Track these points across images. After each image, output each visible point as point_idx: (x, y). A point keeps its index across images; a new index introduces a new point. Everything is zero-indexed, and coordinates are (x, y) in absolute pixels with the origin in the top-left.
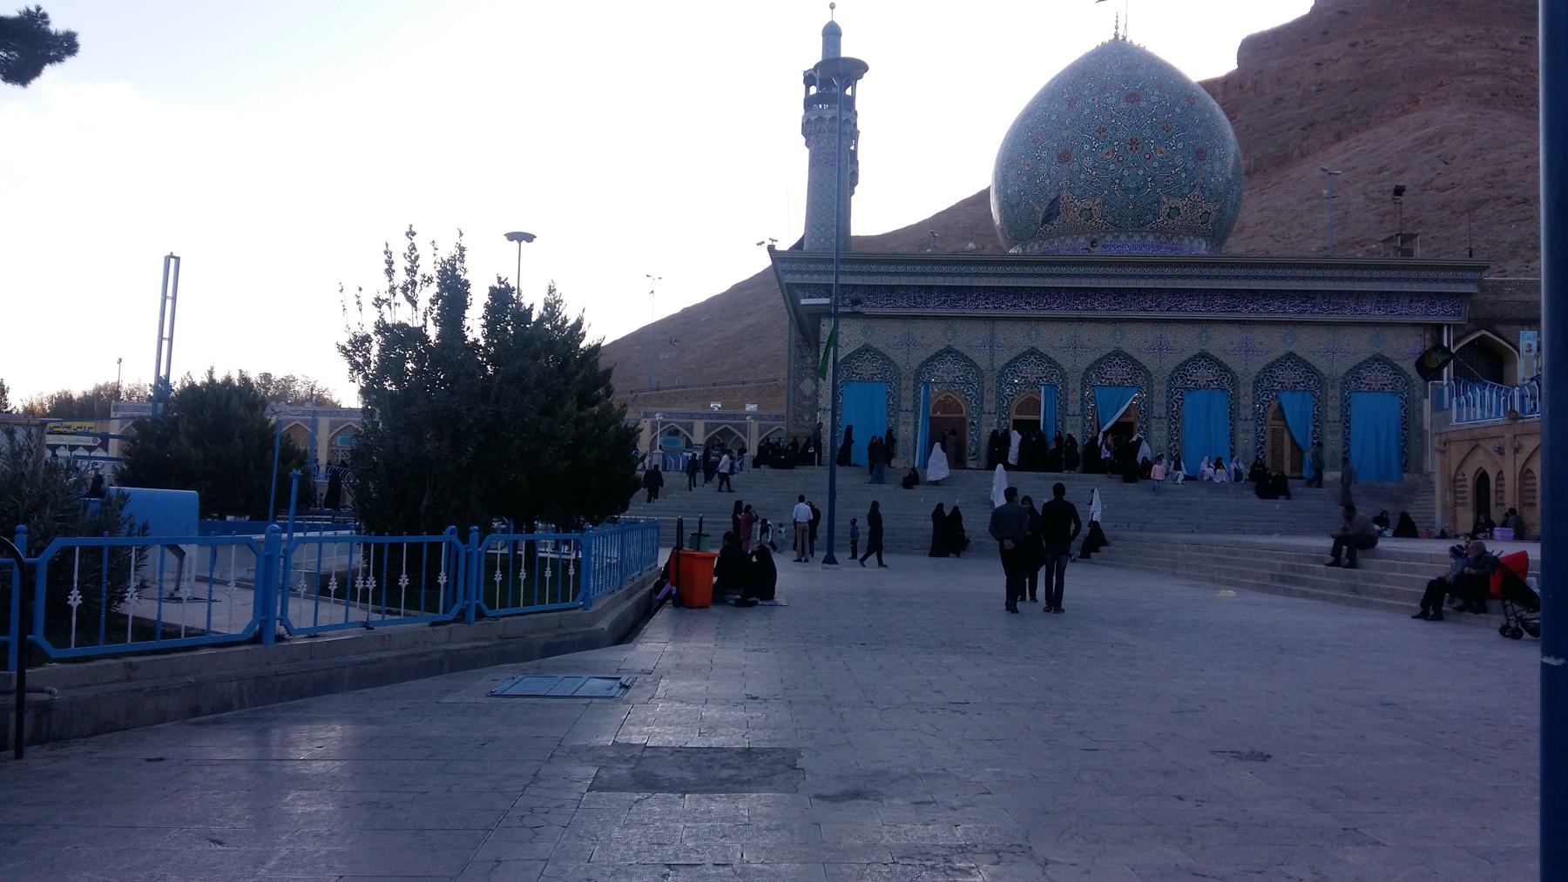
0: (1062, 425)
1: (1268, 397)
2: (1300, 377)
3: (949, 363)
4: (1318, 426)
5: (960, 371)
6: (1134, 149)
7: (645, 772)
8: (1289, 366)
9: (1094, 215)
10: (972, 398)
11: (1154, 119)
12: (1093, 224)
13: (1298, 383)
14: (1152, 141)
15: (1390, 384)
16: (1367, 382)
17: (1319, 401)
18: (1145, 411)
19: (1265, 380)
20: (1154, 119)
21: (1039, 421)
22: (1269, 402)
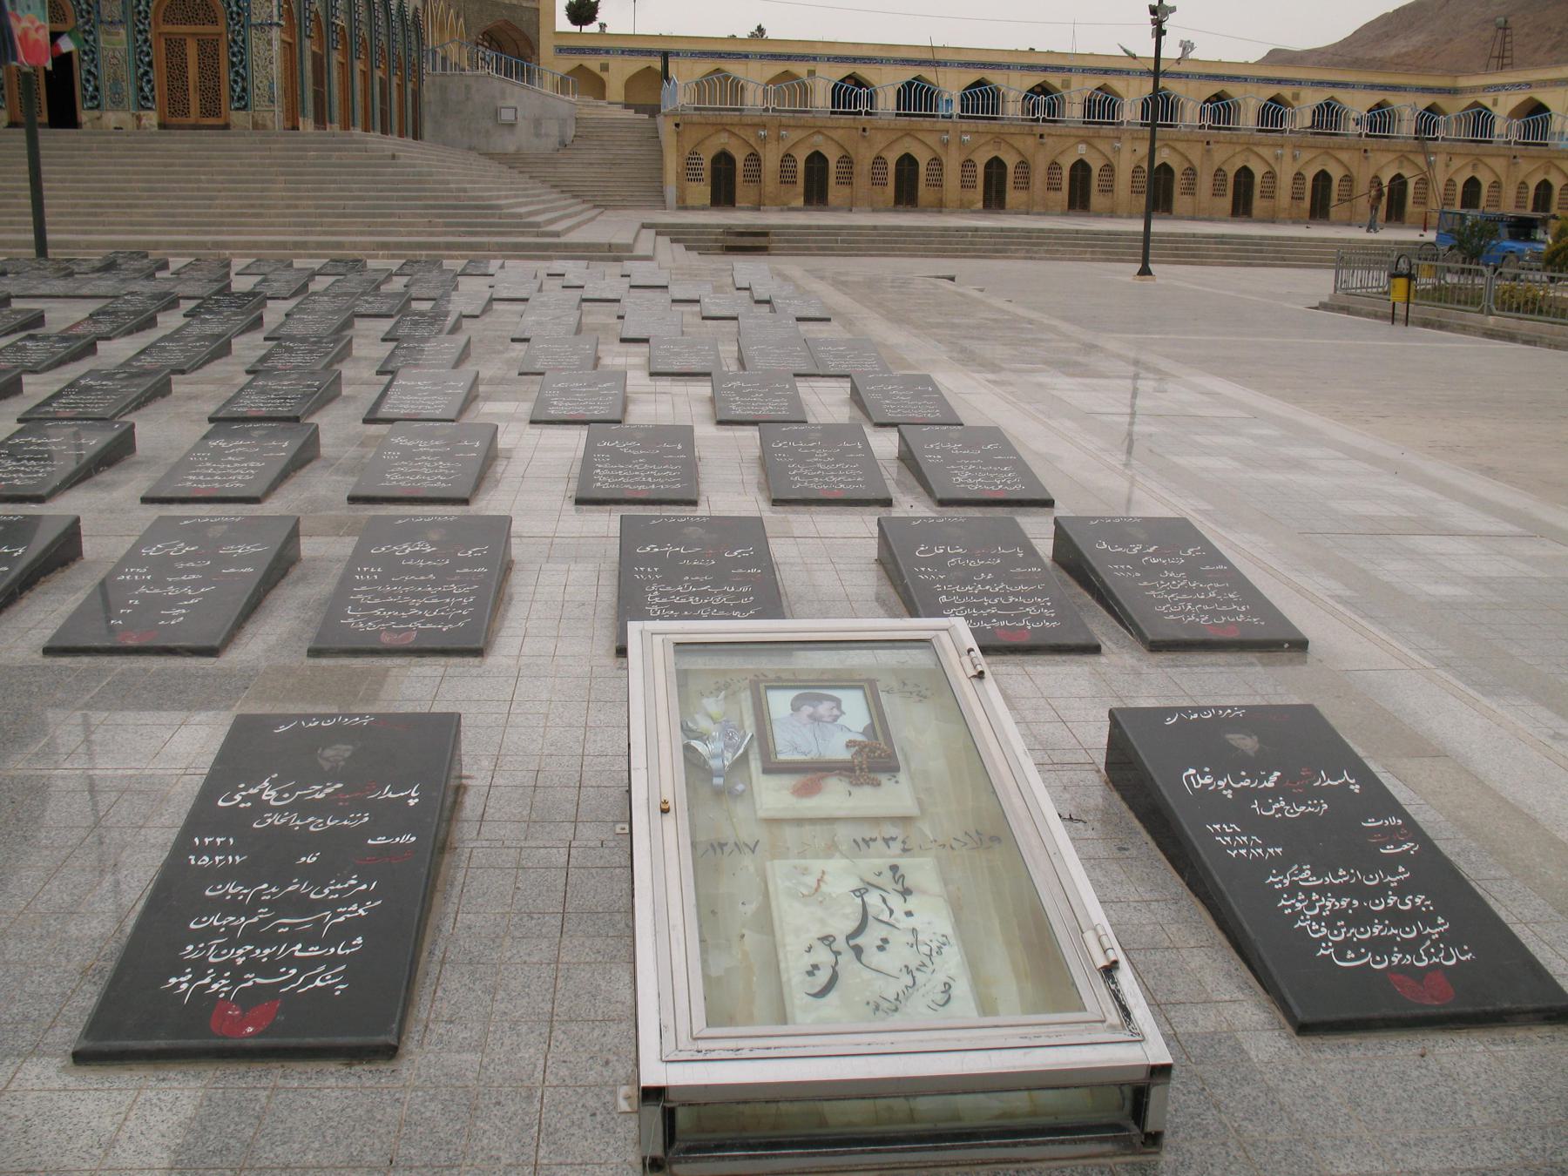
0: (243, 41)
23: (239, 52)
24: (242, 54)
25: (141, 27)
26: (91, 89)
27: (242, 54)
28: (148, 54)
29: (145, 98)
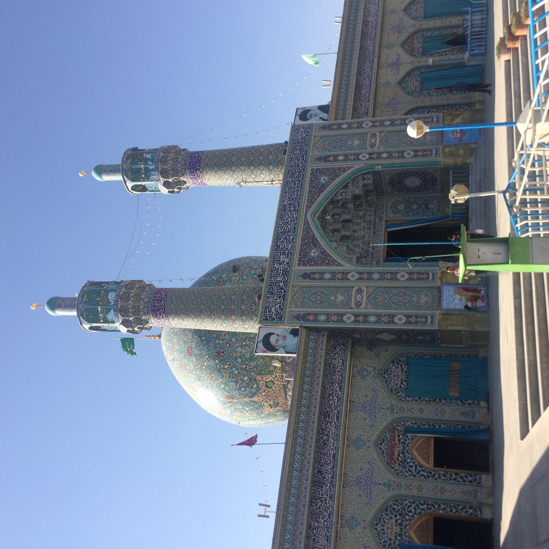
1: (412, 467)
2: (397, 368)
3: (412, 11)
4: (439, 505)
6: (222, 354)
7: (464, 82)
8: (387, 375)
9: (270, 379)
10: (419, 508)
11: (203, 338)
12: (276, 379)
13: (399, 441)
14: (217, 341)
15: (401, 366)
16: (393, 538)
17: (414, 502)
18: (428, 505)
19: (399, 394)
20: (203, 338)
21: (435, 438)
22: (416, 466)
23: (450, 507)
25: (437, 476)
26: (471, 511)
28: (451, 475)
29: (475, 479)
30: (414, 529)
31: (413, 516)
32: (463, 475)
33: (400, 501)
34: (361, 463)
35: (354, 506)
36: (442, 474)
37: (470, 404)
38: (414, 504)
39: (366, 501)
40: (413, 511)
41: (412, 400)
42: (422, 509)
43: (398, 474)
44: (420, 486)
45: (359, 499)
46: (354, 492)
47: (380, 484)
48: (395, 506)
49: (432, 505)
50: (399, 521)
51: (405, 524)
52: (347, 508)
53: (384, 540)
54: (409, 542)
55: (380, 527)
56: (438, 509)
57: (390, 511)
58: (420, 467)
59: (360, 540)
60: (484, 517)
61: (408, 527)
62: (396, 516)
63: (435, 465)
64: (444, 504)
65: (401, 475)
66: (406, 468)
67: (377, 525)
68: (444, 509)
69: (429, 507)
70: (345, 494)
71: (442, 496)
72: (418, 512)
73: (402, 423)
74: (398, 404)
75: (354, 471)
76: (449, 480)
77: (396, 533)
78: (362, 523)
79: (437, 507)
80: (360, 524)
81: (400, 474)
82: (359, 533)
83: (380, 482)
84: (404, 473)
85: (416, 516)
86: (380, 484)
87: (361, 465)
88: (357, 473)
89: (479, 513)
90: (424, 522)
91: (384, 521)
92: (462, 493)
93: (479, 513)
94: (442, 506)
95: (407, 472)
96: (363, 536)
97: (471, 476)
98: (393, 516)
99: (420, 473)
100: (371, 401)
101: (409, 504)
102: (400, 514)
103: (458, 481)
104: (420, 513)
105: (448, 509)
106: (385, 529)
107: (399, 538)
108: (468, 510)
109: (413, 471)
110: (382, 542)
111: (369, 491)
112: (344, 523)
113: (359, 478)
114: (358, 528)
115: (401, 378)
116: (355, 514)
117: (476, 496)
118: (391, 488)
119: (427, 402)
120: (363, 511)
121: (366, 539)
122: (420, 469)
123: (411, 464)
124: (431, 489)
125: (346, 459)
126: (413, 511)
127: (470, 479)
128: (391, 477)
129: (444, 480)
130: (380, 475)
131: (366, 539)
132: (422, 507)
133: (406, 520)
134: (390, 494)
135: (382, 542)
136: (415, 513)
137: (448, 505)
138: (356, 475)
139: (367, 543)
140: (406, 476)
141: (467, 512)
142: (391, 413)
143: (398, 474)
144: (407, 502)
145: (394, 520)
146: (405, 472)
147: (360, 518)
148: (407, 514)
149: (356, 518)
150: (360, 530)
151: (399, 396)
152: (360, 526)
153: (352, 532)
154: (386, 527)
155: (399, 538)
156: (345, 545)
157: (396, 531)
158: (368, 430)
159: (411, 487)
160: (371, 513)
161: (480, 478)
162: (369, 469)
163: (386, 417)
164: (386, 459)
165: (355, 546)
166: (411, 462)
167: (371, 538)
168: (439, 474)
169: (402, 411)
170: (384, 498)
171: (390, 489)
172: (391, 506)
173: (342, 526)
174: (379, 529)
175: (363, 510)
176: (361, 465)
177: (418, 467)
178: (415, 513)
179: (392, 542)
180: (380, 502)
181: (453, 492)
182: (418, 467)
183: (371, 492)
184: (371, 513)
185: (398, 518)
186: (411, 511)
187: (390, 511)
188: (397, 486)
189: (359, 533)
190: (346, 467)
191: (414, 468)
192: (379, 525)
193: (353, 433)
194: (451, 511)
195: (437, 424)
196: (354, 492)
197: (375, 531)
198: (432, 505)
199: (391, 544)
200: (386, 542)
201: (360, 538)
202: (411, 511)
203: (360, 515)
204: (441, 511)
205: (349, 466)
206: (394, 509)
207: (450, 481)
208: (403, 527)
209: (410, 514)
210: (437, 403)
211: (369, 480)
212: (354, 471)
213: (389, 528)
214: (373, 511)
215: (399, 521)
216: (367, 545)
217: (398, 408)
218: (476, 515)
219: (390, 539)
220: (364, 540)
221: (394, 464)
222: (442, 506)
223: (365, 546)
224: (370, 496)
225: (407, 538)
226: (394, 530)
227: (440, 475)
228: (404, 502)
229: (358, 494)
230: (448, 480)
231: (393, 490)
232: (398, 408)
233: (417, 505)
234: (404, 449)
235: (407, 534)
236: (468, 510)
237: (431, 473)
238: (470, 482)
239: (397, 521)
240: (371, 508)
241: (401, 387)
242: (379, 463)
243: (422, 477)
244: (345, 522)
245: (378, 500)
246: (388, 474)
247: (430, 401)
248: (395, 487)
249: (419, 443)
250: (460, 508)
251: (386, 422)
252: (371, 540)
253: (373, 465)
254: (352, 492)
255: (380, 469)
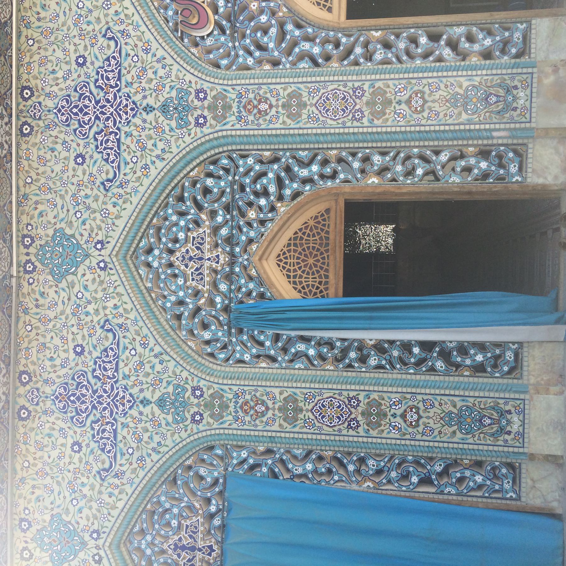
4: (366, 159)
5: (197, 223)
17: (276, 160)
18: (325, 162)
22: (282, 25)
24: (408, 158)
25: (358, 50)
26: (484, 165)
27: (408, 158)
28: (414, 41)
29: (506, 43)
30: (277, 250)
31: (273, 209)
32: (460, 30)
33: (225, 161)
34: (77, 40)
35: (62, 197)
36: (378, 41)
37: (487, 55)
38: (276, 167)
39: (104, 176)
40: (272, 189)
41: (259, 62)
42: (305, 181)
43: (218, 66)
44: (296, 95)
45: (80, 173)
46: (59, 147)
47: (148, 109)
48: (210, 182)
49: (340, 160)
50: (224, 232)
51: (244, 238)
52: (41, 207)
53: (173, 298)
54: (262, 296)
55: (160, 258)
56: (363, 171)
57: (195, 201)
58: (299, 26)
59: (90, 308)
60: (533, 179)
61: (254, 247)
62: (213, 214)
63: (350, 15)
64: (383, 154)
65: (228, 67)
66: (244, 36)
67: (149, 251)
68: (383, 170)
69: (328, 171)
70: (28, 159)
71: (374, 433)
72: (288, 192)
73: (225, 161)
74: (202, 383)
75: (54, 72)
76: (405, 58)
77: (216, 272)
78: (92, 251)
79: (356, 165)
80: (87, 256)
81: (224, 62)
82: (86, 287)
83: (150, 101)
84: (237, 56)
85: (282, 208)
86: (148, 109)
87: (79, 337)
88: (65, 79)
89: (513, 168)
90: (312, 223)
91: (171, 236)
92: (453, 100)
93: (513, 168)
94: (377, 159)
95: (250, 53)
96: (100, 295)
97: (490, 33)
98: (204, 217)
99: (297, 50)
100: (98, 373)
101: (257, 167)
102: (227, 208)
103: (440, 59)
104: (296, 195)
105: (399, 168)
106: (177, 263)
107: (223, 287)
108: (468, 473)
109: (271, 45)
110: (168, 305)
111: (108, 427)
112: (33, 259)
113: (75, 97)
114: (80, 271)
115: (210, 268)
116: (70, 224)
117: (509, 107)
118: (188, 416)
119: (316, 64)
120: (94, 212)
121: (110, 304)
122: (297, 33)
123: (264, 18)
124: (335, 104)
125: (24, 31)
126: (272, 189)
127: (488, 42)
128: (188, 77)
129: (379, 367)
130: (150, 75)
131: (110, 304)
132: (304, 173)
133: (249, 224)
134: (188, 139)
135: (168, 305)
136: (281, 198)
137: (398, 153)
138: (63, 86)
139: (115, 317)
140: (248, 68)
141: (468, 170)
142: (180, 127)
143: (218, 66)
144: (250, 161)
145: (205, 229)
146: (241, 52)
147: (86, 234)
148: (250, 204)
149: (73, 236)
150: (89, 276)
151: (209, 52)
152: (87, 262)
153: (64, 284)
154: (178, 254)
155: (223, 287)
156: (43, 328)
157: (214, 265)
158: (92, 488)
159: (263, 106)
160: (123, 213)
161: (526, 38)
162: (108, 59)
163: (157, 438)
164: (170, 13)
165: (75, 329)
166: (262, 12)
167: (126, 298)
168: (366, 45)
169: (220, 112)
170: (167, 156)
171: (184, 420)
172: (194, 184)
173: (29, 267)
174: (155, 264)
175: (94, 206)
176: (81, 48)
177: (289, 27)
178: (281, 198)
179: (203, 301)
180: (153, 172)
181: (417, 102)
182: (289, 27)
183: (119, 140)
184: (123, 213)
185: (220, 219)
186: (265, 193)
187: (195, 201)
188: (212, 108)
189: (86, 287)
190: (27, 60)
191: (273, 31)
192: (156, 252)
193: (41, 215)
194: (410, 173)
195: (354, 155)
196: (59, 147)
197: (143, 271)
198: (340, 160)
199: (198, 310)
200: (181, 303)
201: (89, 302)
202: (265, 193)
203: (87, 226)
204: (375, 180)
205: (36, 57)
206: (207, 191)
207: (409, 65)
208: (238, 249)
209: (263, 202)
210: (356, 63)
211: (111, 97)
212: (54, 72)
213: (191, 259)
214: (130, 208)
215: (224, 232)
216: (116, 321)
217: (206, 103)
218: (501, 179)
219: (197, 294)
220: (105, 308)
221: (198, 26)
222: (377, 159)
223: (109, 34)
224: (117, 155)
225: (251, 285)
226: (207, 264)
227: (371, 47)
228: (241, 162)
229: (70, 441)
230: (399, 60)
231: (197, 124)
232: (206, 103)
233: (288, 169)
234: (232, 264)
235: (253, 272)
236: (472, 161)
237: (337, 45)
238: (487, 55)
239: (216, 230)
240: (120, 196)
241: (212, 303)
242: (143, 28)
243: (304, 65)
244: (36, 255)
245: (146, 167)
246: (176, 67)
247: (323, 358)
248: (206, 113)
249: (289, 234)
250: (444, 157)
251: (160, 165)
252: (129, 306)
253: (120, 333)
254: (53, 150)
255: (147, 51)
